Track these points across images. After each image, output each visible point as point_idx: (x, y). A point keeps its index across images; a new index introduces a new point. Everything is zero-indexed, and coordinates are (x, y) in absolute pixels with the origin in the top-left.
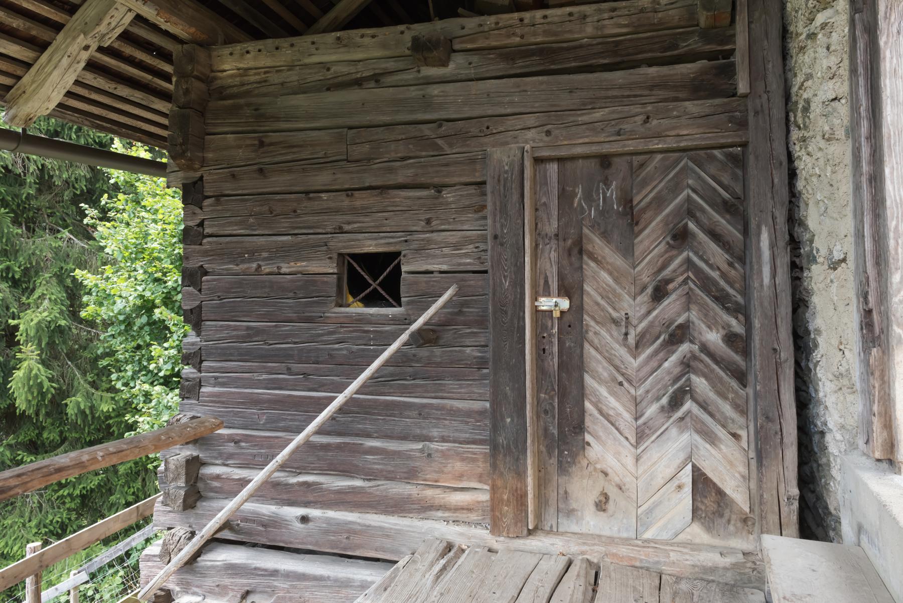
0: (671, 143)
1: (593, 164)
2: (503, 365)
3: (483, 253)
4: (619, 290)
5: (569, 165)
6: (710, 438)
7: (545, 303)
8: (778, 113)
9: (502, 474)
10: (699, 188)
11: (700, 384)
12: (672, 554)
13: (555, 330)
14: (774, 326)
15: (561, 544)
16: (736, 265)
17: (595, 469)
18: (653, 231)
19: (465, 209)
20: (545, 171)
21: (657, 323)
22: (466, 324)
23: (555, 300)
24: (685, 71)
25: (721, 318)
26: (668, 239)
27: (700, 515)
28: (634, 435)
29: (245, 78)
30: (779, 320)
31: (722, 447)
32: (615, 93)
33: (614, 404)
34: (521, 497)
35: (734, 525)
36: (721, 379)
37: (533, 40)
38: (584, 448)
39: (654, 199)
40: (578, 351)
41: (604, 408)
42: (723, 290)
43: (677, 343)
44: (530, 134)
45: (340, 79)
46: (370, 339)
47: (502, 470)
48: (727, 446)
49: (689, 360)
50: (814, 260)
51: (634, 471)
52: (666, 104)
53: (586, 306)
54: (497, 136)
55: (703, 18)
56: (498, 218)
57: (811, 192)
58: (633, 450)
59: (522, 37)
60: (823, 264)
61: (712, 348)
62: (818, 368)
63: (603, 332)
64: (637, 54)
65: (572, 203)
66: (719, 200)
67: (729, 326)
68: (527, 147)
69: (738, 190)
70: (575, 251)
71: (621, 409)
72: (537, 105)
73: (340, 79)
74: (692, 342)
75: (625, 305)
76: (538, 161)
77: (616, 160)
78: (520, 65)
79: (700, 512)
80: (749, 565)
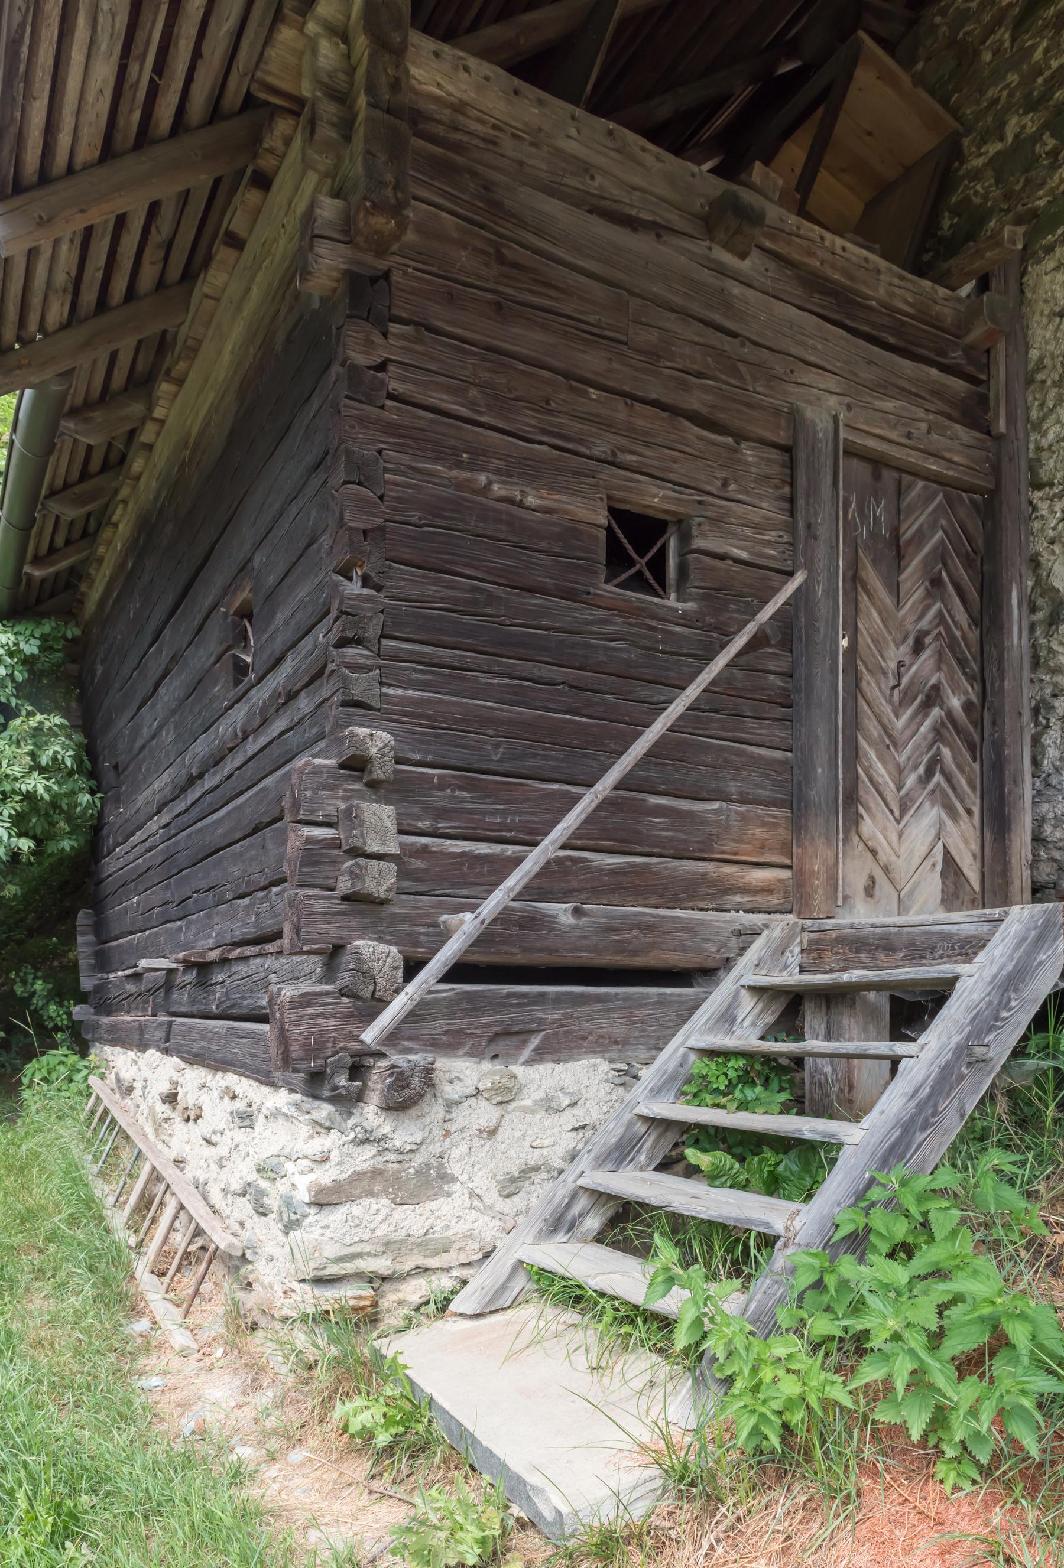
26: (927, 583)
29: (460, 118)
45: (608, 203)
46: (658, 641)
59: (822, 262)
73: (608, 203)
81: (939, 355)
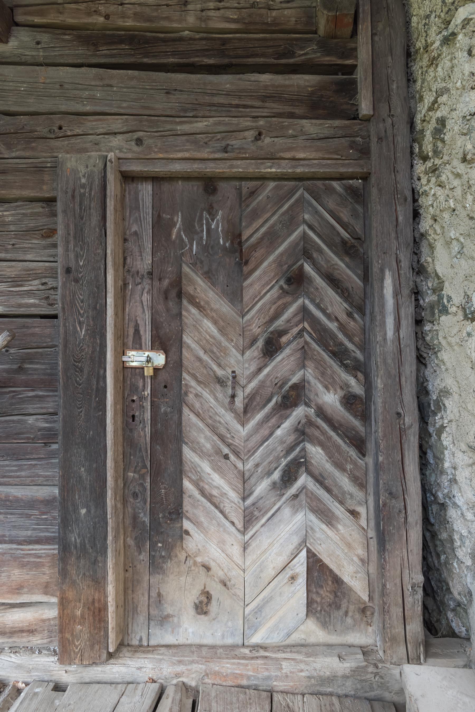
0: (285, 168)
1: (196, 188)
2: (77, 438)
3: (52, 292)
4: (225, 343)
5: (166, 187)
6: (327, 517)
7: (135, 358)
8: (402, 141)
9: (73, 583)
10: (316, 224)
11: (316, 453)
12: (284, 664)
13: (148, 392)
14: (398, 387)
15: (150, 666)
16: (356, 316)
17: (195, 563)
18: (265, 273)
19: (29, 232)
20: (137, 194)
21: (268, 383)
22: (29, 385)
23: (147, 354)
24: (302, 83)
25: (340, 377)
26: (282, 282)
27: (316, 609)
28: (242, 518)
30: (403, 379)
31: (340, 527)
32: (221, 100)
33: (218, 482)
34: (100, 611)
35: (352, 617)
36: (338, 448)
37: (120, 23)
38: (181, 538)
39: (265, 234)
40: (176, 417)
41: (206, 487)
42: (341, 344)
43: (291, 407)
44: (116, 141)
47: (74, 577)
48: (344, 525)
49: (304, 426)
50: (445, 311)
51: (241, 563)
52: (281, 120)
53: (185, 362)
54: (73, 140)
55: (322, 25)
56: (71, 246)
57: (439, 231)
58: (239, 536)
59: (107, 17)
60: (455, 314)
61: (329, 411)
62: (444, 435)
63: (206, 394)
64: (248, 57)
65: (170, 235)
66: (337, 240)
67: (348, 385)
68: (111, 155)
69: (358, 229)
70: (173, 294)
71: (226, 488)
72: (125, 105)
74: (307, 405)
75: (232, 361)
76: (128, 178)
77: (223, 186)
78: (105, 53)
79: (315, 605)
80: (371, 669)
81: (281, 56)
